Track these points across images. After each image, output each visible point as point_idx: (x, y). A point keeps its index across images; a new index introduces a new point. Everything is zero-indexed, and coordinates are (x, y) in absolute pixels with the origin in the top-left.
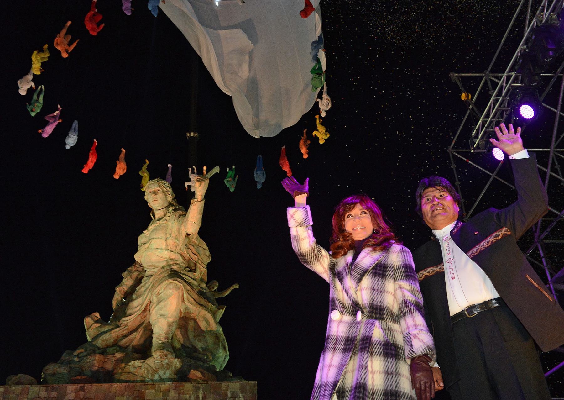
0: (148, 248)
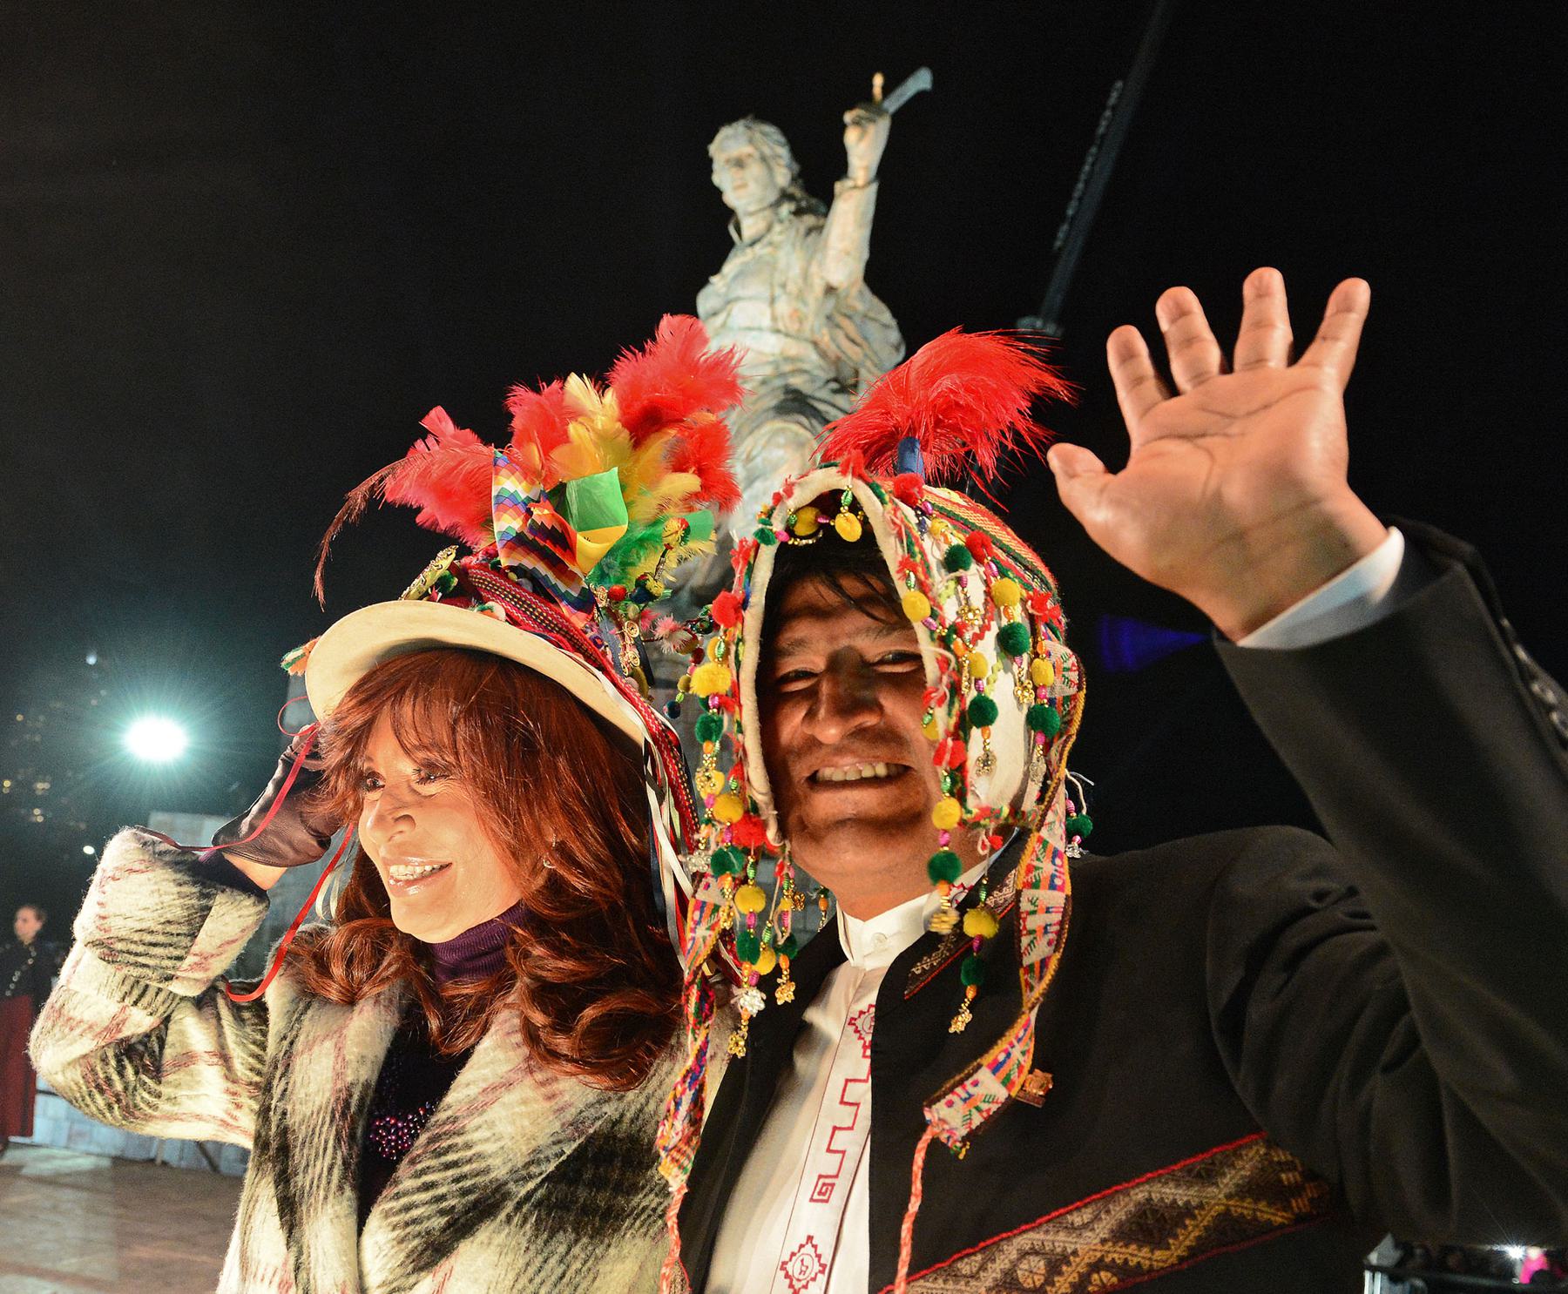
0: (724, 325)
